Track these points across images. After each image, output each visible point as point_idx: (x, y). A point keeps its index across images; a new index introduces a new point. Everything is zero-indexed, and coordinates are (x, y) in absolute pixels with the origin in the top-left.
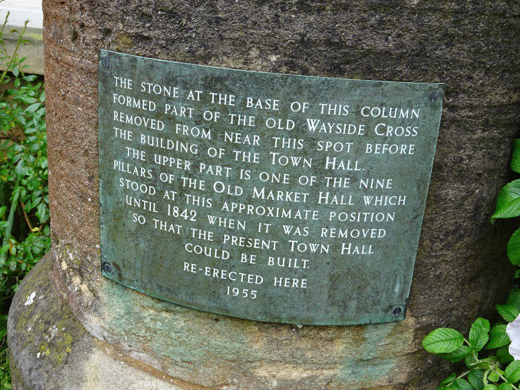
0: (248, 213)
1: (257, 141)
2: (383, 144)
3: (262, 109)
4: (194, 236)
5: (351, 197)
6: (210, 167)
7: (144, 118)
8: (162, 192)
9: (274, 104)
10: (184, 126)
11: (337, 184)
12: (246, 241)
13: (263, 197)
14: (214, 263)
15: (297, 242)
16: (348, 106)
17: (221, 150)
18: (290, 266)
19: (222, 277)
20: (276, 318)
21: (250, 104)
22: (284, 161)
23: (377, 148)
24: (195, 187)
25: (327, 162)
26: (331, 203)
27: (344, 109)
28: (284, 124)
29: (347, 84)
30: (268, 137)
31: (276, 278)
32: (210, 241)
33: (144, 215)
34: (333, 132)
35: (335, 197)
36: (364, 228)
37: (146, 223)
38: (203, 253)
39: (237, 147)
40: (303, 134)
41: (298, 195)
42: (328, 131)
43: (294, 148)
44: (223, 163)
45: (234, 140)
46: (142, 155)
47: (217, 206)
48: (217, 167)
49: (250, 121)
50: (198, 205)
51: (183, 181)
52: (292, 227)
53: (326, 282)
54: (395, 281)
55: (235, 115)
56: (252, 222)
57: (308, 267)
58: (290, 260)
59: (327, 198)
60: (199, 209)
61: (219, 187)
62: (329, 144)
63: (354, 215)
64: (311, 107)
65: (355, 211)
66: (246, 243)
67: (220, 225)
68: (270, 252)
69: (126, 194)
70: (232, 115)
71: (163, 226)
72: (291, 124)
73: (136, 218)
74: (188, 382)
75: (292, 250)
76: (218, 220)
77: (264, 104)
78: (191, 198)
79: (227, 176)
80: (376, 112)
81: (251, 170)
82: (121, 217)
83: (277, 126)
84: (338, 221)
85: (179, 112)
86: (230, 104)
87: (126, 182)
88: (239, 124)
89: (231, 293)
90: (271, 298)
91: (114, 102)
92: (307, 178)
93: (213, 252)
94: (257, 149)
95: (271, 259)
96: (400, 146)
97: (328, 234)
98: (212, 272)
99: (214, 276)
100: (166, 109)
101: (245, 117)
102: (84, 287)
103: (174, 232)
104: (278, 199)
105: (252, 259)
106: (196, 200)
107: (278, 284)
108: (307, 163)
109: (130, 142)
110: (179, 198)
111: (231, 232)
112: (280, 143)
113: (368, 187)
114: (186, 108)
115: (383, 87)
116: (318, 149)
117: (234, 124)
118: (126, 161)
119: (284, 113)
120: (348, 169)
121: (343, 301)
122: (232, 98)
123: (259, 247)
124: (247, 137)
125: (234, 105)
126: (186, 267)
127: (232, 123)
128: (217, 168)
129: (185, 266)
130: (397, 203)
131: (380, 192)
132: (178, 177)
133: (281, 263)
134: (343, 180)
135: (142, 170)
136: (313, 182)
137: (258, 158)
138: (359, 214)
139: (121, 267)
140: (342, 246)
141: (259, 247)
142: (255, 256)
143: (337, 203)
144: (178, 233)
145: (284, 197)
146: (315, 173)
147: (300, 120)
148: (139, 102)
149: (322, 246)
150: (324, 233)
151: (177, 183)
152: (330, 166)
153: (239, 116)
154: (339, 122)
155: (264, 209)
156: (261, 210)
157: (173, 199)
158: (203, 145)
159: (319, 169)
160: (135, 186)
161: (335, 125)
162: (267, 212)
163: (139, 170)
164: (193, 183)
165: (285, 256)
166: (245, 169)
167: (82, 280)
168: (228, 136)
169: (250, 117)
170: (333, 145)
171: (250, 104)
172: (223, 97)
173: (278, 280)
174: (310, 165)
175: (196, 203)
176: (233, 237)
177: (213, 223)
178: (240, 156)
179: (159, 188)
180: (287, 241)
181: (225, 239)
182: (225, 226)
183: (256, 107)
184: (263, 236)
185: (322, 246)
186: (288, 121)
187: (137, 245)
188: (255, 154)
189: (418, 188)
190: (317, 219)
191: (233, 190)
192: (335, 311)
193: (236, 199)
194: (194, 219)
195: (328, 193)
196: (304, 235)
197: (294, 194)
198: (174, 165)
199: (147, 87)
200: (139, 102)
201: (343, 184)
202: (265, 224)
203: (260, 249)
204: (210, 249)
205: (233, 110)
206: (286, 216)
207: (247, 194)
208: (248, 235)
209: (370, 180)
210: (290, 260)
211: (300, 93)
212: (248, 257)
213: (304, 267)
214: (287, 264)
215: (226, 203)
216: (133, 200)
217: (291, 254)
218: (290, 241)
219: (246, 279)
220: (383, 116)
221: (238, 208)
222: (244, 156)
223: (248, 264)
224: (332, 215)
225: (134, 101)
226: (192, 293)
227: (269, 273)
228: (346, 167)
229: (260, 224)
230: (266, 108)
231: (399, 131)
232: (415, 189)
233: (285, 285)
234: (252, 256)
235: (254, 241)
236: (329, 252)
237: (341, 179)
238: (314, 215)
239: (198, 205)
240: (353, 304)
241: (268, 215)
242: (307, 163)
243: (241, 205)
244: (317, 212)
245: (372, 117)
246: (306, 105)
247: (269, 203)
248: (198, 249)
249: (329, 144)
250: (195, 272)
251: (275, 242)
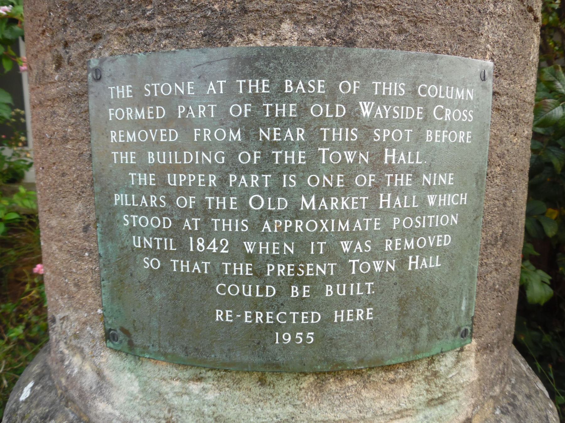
0: (297, 231)
1: (301, 135)
2: (442, 130)
3: (304, 94)
4: (226, 273)
5: (414, 197)
6: (243, 177)
7: (151, 131)
8: (182, 221)
9: (319, 86)
10: (205, 130)
11: (399, 182)
12: (296, 268)
13: (314, 208)
14: (256, 305)
15: (358, 261)
16: (404, 84)
17: (255, 153)
18: (352, 294)
19: (268, 322)
20: (340, 365)
21: (289, 89)
22: (335, 157)
23: (437, 136)
24: (224, 208)
25: (386, 156)
26: (394, 207)
27: (400, 87)
28: (332, 111)
29: (400, 57)
30: (315, 129)
31: (336, 312)
32: (248, 276)
33: (158, 257)
34: (390, 117)
35: (398, 199)
36: (430, 235)
37: (161, 267)
38: (240, 294)
39: (276, 145)
40: (356, 121)
41: (355, 200)
42: (384, 115)
43: (347, 140)
44: (260, 169)
45: (272, 137)
46: (151, 179)
47: (255, 230)
48: (252, 176)
49: (291, 110)
50: (230, 230)
51: (207, 202)
52: (351, 242)
53: (394, 308)
54: (461, 297)
55: (271, 105)
56: (302, 242)
57: (373, 292)
58: (352, 285)
59: (389, 201)
60: (231, 236)
61: (256, 202)
62: (387, 133)
63: (419, 219)
64: (363, 86)
65: (419, 214)
66: (296, 271)
67: (261, 253)
68: (327, 279)
69: (133, 234)
70: (268, 105)
71: (185, 267)
72: (341, 111)
73: (148, 263)
75: (353, 272)
76: (257, 246)
77: (306, 86)
78: (220, 223)
79: (266, 186)
80: (433, 92)
81: (297, 174)
82: (127, 267)
83: (324, 113)
84: (403, 229)
85: (196, 113)
86: (263, 91)
87: (132, 218)
88: (277, 116)
89: (281, 340)
90: (331, 339)
91: (110, 119)
92: (364, 177)
93: (254, 289)
94: (302, 145)
95: (329, 288)
96: (458, 133)
97: (393, 246)
98: (254, 316)
99: (257, 322)
100: (180, 112)
101: (284, 105)
102: (87, 367)
103: (199, 272)
104: (332, 208)
105: (305, 291)
106: (227, 225)
107: (339, 319)
108: (364, 157)
109: (134, 166)
110: (203, 225)
111: (276, 259)
112: (329, 134)
113: (432, 184)
114: (206, 106)
115: (438, 60)
116: (375, 140)
117: (270, 117)
118: (129, 191)
119: (332, 96)
120: (409, 162)
121: (414, 330)
122: (266, 83)
123: (313, 274)
124: (289, 131)
125: (268, 92)
126: (219, 316)
127: (267, 115)
128: (252, 178)
129: (217, 315)
130: (459, 203)
131: (443, 189)
132: (202, 198)
133: (341, 292)
134: (405, 176)
135: (151, 199)
136: (372, 182)
137: (304, 157)
138: (424, 217)
139: (131, 330)
140: (409, 260)
141: (313, 274)
142: (309, 287)
143: (400, 206)
144: (206, 272)
145: (339, 205)
146: (374, 171)
147: (351, 103)
148: (143, 111)
149: (388, 263)
150: (388, 246)
151: (200, 207)
152: (390, 160)
153: (277, 105)
154: (395, 104)
155: (315, 222)
156: (312, 226)
157: (196, 229)
158: (232, 149)
159: (377, 165)
160: (143, 222)
161: (392, 108)
162: (320, 226)
163: (148, 199)
164: (221, 202)
165: (346, 282)
166: (289, 174)
167: (84, 358)
168: (263, 132)
169: (291, 105)
170: (391, 133)
171: (289, 89)
172: (253, 83)
173: (339, 313)
174: (367, 161)
175: (227, 228)
176: (279, 265)
177: (251, 252)
178: (282, 157)
179: (175, 217)
180: (346, 261)
181: (269, 270)
182: (267, 253)
183: (297, 92)
184: (318, 258)
185: (388, 263)
186: (337, 106)
187: (150, 299)
188: (300, 152)
189: (477, 183)
190: (379, 229)
191: (274, 204)
192: (406, 344)
193: (280, 215)
194: (226, 250)
195: (389, 195)
196: (365, 251)
197: (351, 199)
198: (195, 183)
199: (152, 89)
200: (143, 111)
201: (405, 181)
202: (318, 243)
203: (315, 276)
204: (250, 286)
205: (269, 98)
206: (343, 229)
207: (293, 207)
208: (297, 261)
209: (433, 176)
210: (352, 285)
211: (349, 69)
212: (300, 289)
213: (369, 293)
214: (348, 291)
215: (267, 223)
216: (142, 240)
217: (352, 277)
218: (350, 261)
219: (299, 319)
220: (440, 97)
221: (283, 226)
222: (286, 157)
223: (301, 298)
224: (396, 221)
225: (137, 111)
226: (229, 350)
227: (328, 306)
228: (407, 160)
229: (312, 243)
230: (309, 91)
231: (457, 115)
232: (474, 185)
233: (348, 320)
234: (304, 287)
235: (306, 266)
236: (395, 269)
237: (402, 175)
238: (376, 224)
239: (230, 230)
240: (424, 331)
241: (322, 231)
242: (364, 157)
243: (286, 221)
244: (379, 219)
245: (430, 97)
246: (357, 84)
247: (322, 214)
248: (234, 290)
249: (386, 132)
250: (231, 321)
251: (332, 265)
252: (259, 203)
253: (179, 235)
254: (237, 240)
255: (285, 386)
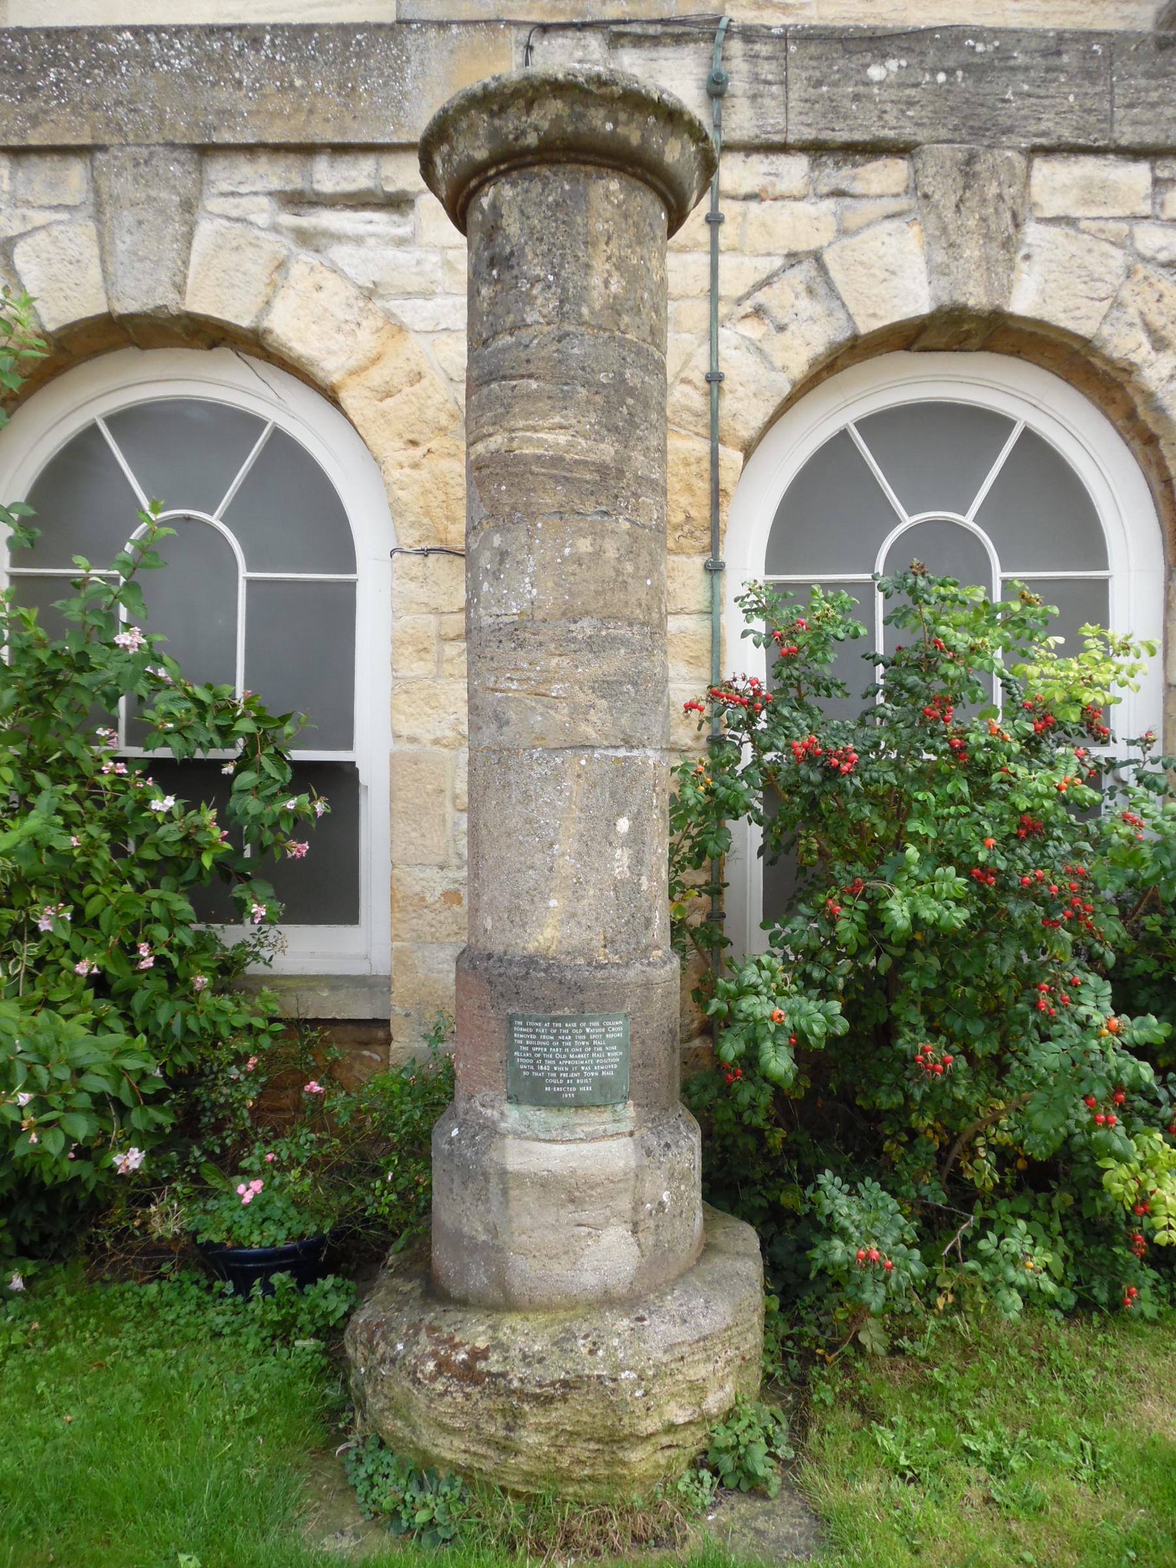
56: (570, 1067)
74: (493, 161)
119: (578, 1027)
159: (591, 1045)
227: (578, 1086)
252: (558, 1056)
253: (535, 1065)
254: (552, 1066)
255: (566, 1111)
